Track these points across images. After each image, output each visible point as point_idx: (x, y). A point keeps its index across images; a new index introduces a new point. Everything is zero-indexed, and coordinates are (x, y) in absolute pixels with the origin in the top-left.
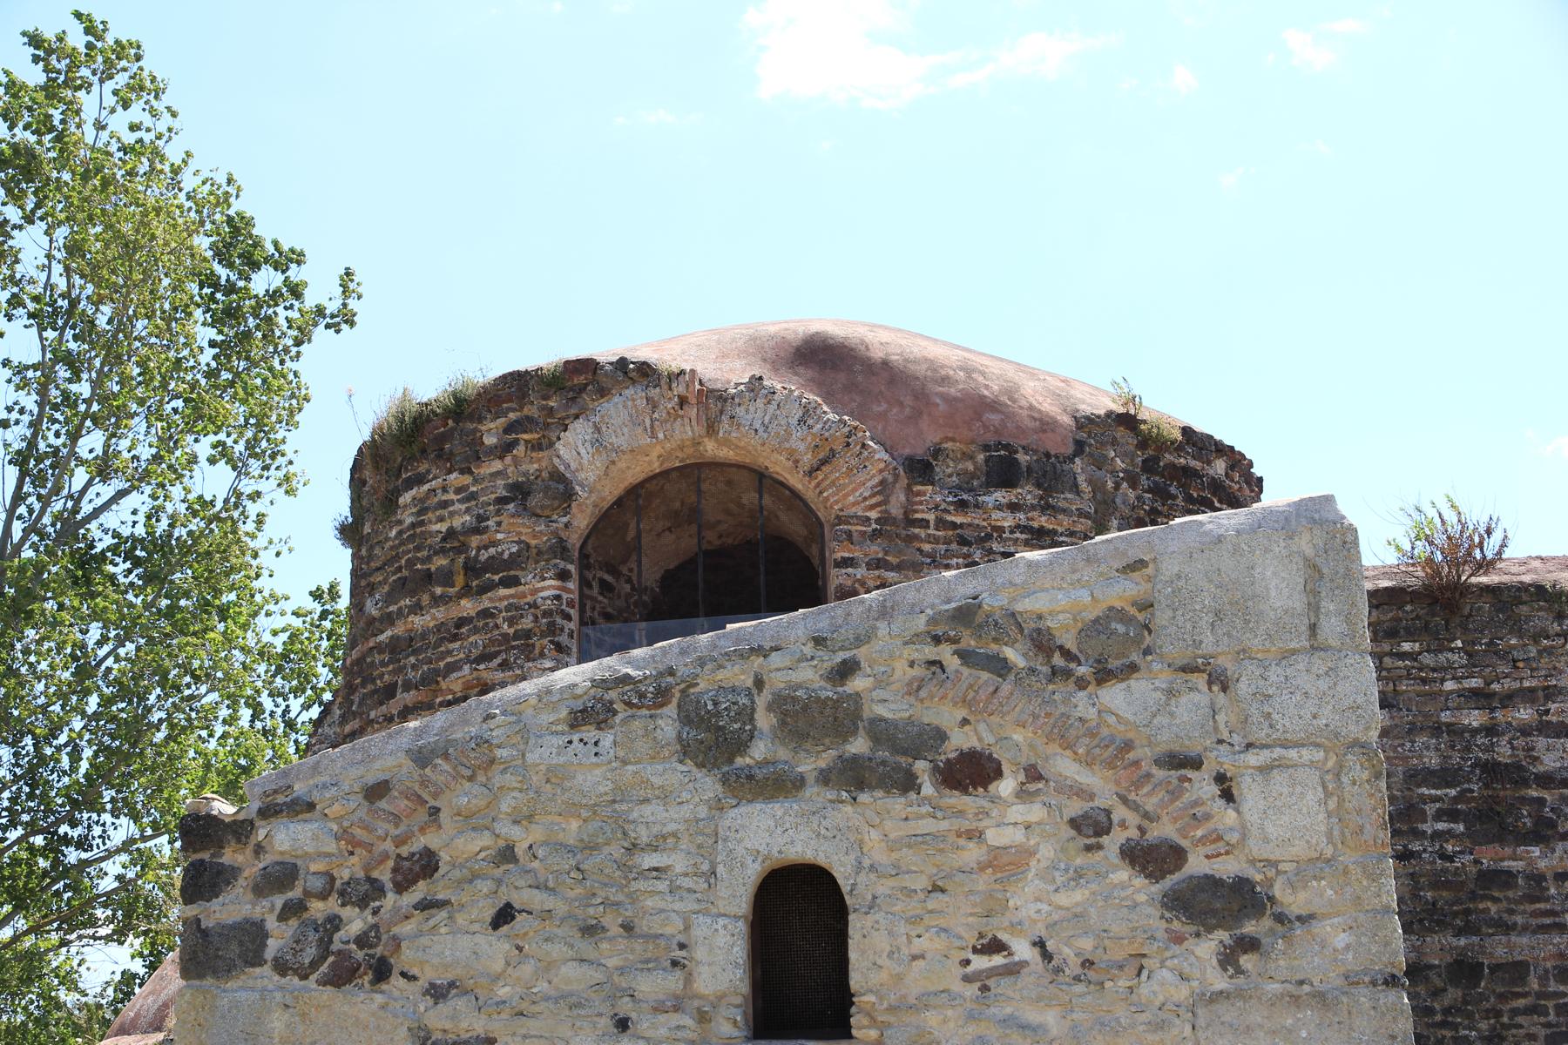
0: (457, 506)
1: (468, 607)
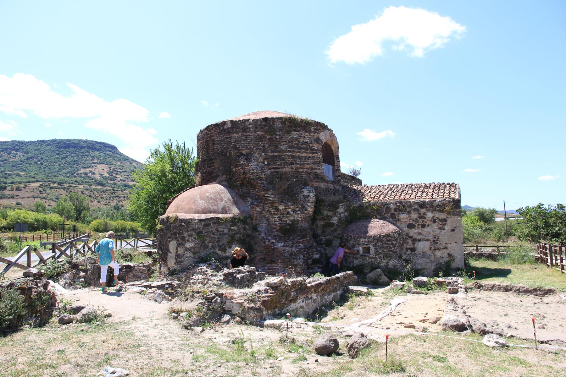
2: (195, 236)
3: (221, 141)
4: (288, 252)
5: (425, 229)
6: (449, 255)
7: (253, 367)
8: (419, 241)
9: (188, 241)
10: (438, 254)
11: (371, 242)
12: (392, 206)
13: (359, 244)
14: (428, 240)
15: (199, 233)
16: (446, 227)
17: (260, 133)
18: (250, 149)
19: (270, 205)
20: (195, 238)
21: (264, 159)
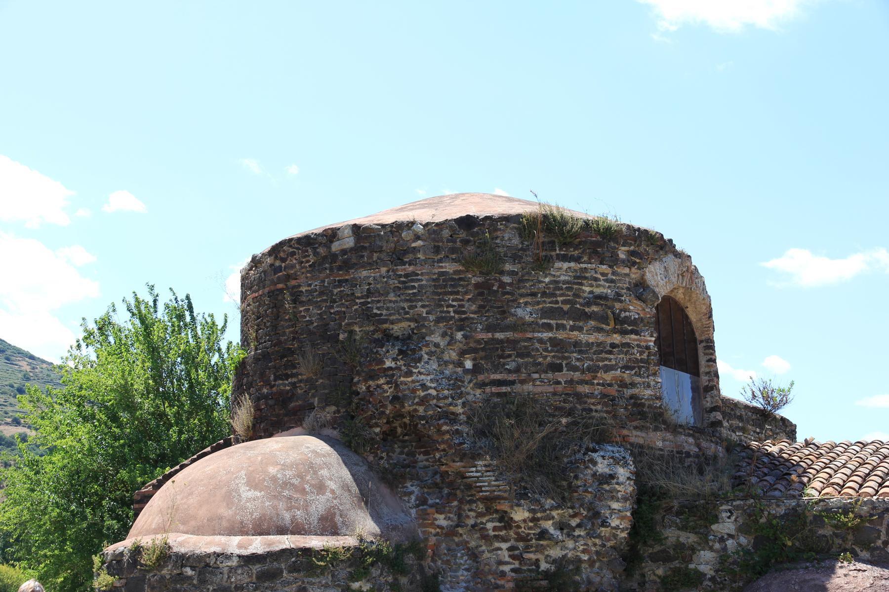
0: (602, 283)
1: (617, 338)
3: (322, 293)
17: (449, 267)
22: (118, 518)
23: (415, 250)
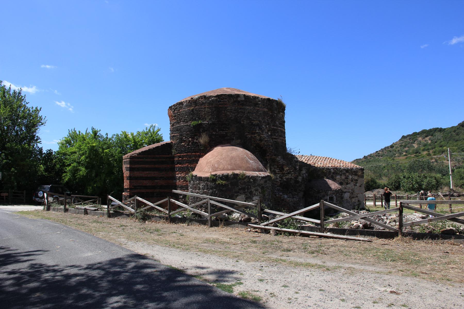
2: (260, 190)
3: (235, 110)
4: (292, 201)
5: (348, 186)
6: (359, 201)
7: (442, 270)
8: (345, 192)
9: (255, 195)
10: (353, 200)
11: (333, 193)
12: (332, 171)
13: (327, 195)
14: (349, 192)
15: (262, 188)
16: (357, 185)
17: (266, 110)
18: (260, 121)
19: (276, 167)
20: (259, 192)
21: (268, 131)
22: (300, 170)
23: (259, 104)
